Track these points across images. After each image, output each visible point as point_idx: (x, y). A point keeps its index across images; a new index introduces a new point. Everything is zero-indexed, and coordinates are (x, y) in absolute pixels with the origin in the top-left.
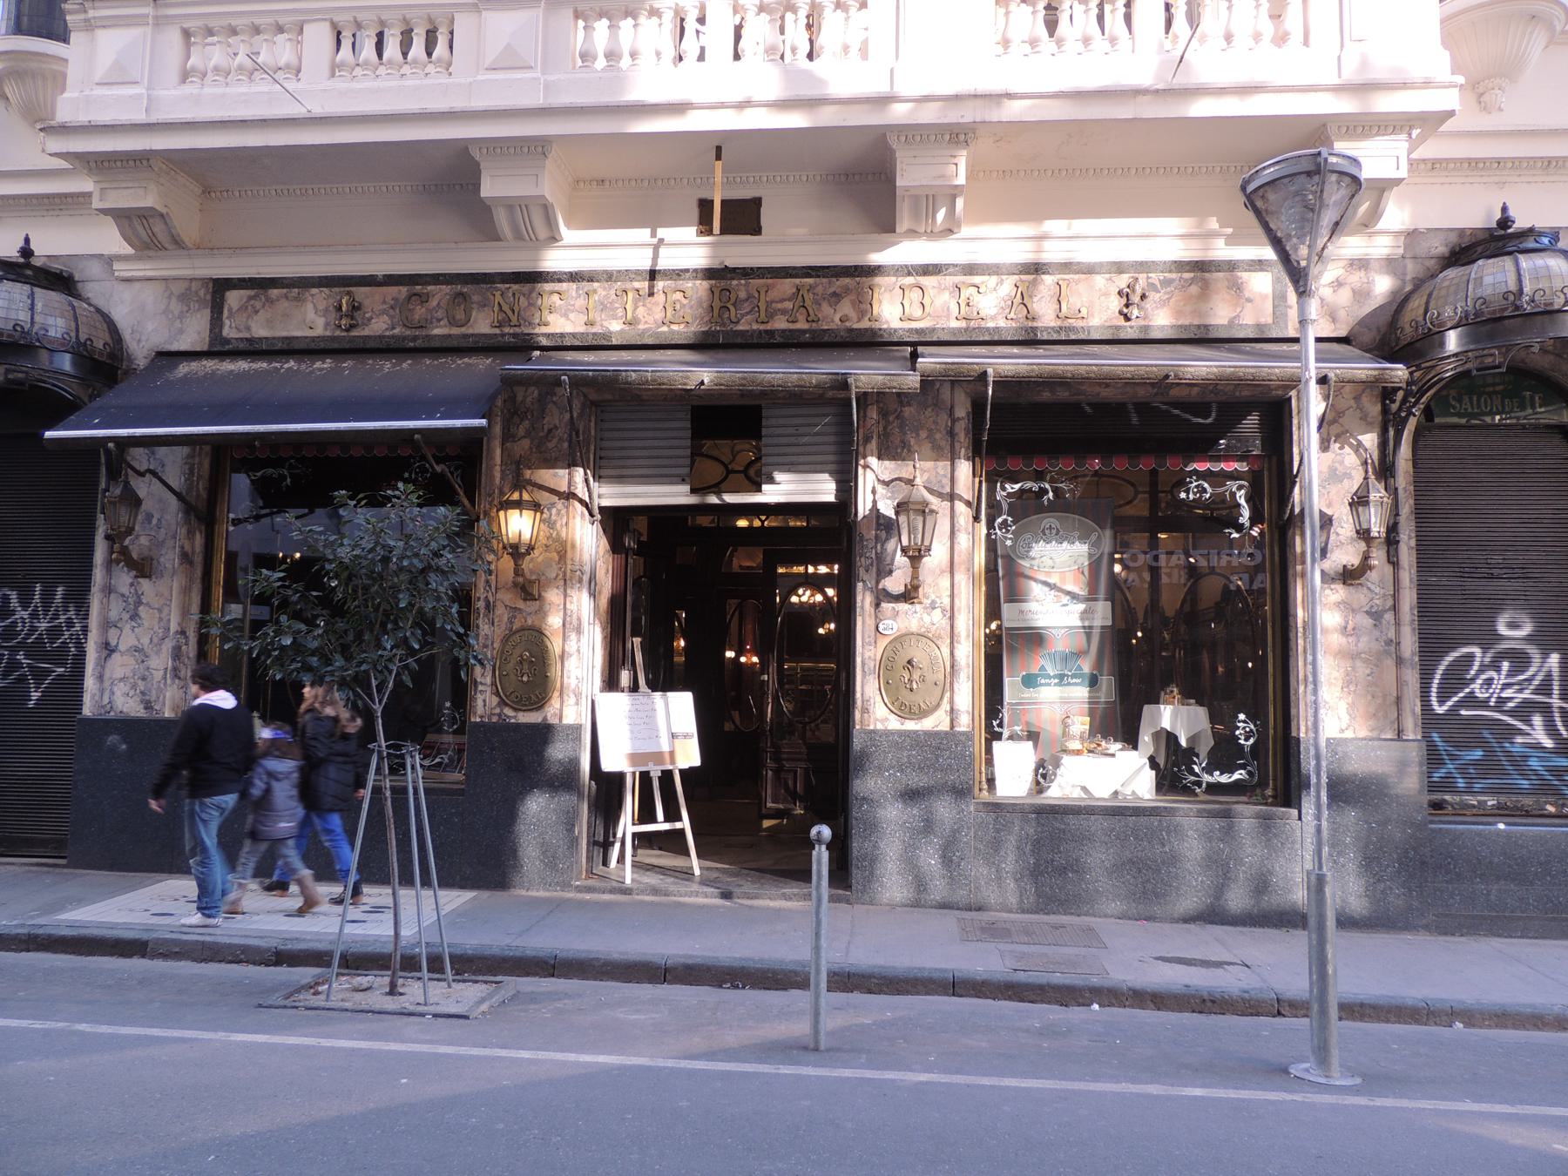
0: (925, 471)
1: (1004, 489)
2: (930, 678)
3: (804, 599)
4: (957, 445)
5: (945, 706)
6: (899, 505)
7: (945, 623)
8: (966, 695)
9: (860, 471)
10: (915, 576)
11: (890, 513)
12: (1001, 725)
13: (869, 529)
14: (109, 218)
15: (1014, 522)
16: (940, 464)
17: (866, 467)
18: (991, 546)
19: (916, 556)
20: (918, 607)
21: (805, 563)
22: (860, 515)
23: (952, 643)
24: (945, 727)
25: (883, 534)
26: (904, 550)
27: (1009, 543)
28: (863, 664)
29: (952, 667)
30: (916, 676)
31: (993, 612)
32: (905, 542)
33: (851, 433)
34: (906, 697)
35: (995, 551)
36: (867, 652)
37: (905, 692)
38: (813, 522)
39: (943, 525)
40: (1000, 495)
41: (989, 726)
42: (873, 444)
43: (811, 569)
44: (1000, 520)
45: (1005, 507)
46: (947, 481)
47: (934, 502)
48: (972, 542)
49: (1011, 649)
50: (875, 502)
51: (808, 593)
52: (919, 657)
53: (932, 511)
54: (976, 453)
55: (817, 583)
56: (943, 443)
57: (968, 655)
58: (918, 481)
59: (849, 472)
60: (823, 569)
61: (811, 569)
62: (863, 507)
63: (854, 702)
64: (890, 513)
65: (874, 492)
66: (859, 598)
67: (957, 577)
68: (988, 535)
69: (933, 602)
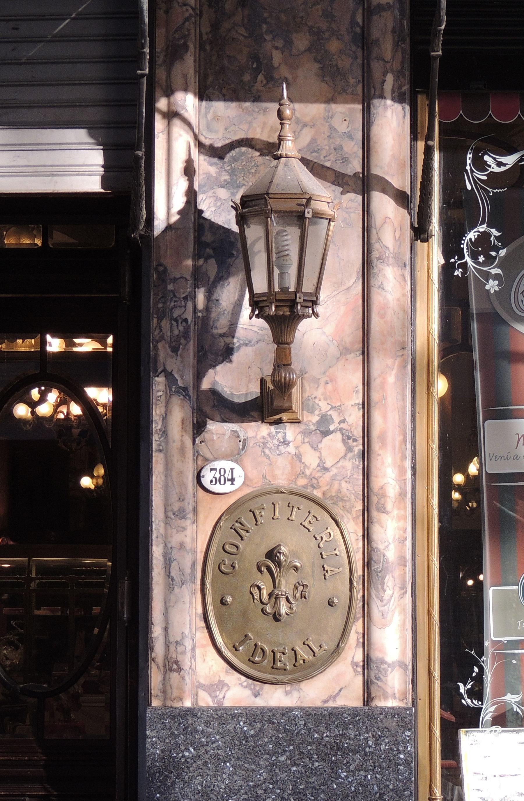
0: (308, 125)
1: (480, 165)
2: (318, 591)
3: (44, 410)
4: (377, 67)
5: (353, 652)
6: (245, 201)
7: (352, 467)
8: (397, 633)
9: (159, 124)
10: (282, 361)
11: (227, 219)
12: (477, 693)
13: (179, 257)
14: (188, 157)
15: (504, 240)
16: (340, 109)
17: (171, 115)
18: (454, 291)
19: (284, 312)
20: (290, 432)
21: (39, 329)
22: (160, 222)
23: (366, 510)
24: (351, 699)
25: (211, 268)
26: (257, 304)
27: (492, 286)
28: (168, 561)
29: (368, 564)
30: (286, 586)
31: (459, 438)
32: (260, 286)
33: (133, 37)
34: (267, 635)
35: (465, 304)
36: (180, 538)
37: (266, 623)
38: (59, 237)
39: (345, 255)
40: (473, 178)
41: (450, 698)
42: (189, 64)
43: (55, 345)
44: (472, 235)
45: (484, 207)
46: (353, 148)
47: (323, 195)
48: (410, 291)
49: (504, 527)
50: (191, 195)
51: (53, 396)
52: (293, 544)
53: (318, 215)
54: (415, 90)
55: (69, 374)
56: (345, 63)
57: (402, 538)
58: (289, 147)
59: (134, 124)
60: (86, 345)
61: (55, 345)
62: (166, 204)
63: (148, 647)
64: (227, 219)
65: (189, 171)
66: (157, 412)
67: (378, 364)
68: (447, 270)
69: (325, 419)
